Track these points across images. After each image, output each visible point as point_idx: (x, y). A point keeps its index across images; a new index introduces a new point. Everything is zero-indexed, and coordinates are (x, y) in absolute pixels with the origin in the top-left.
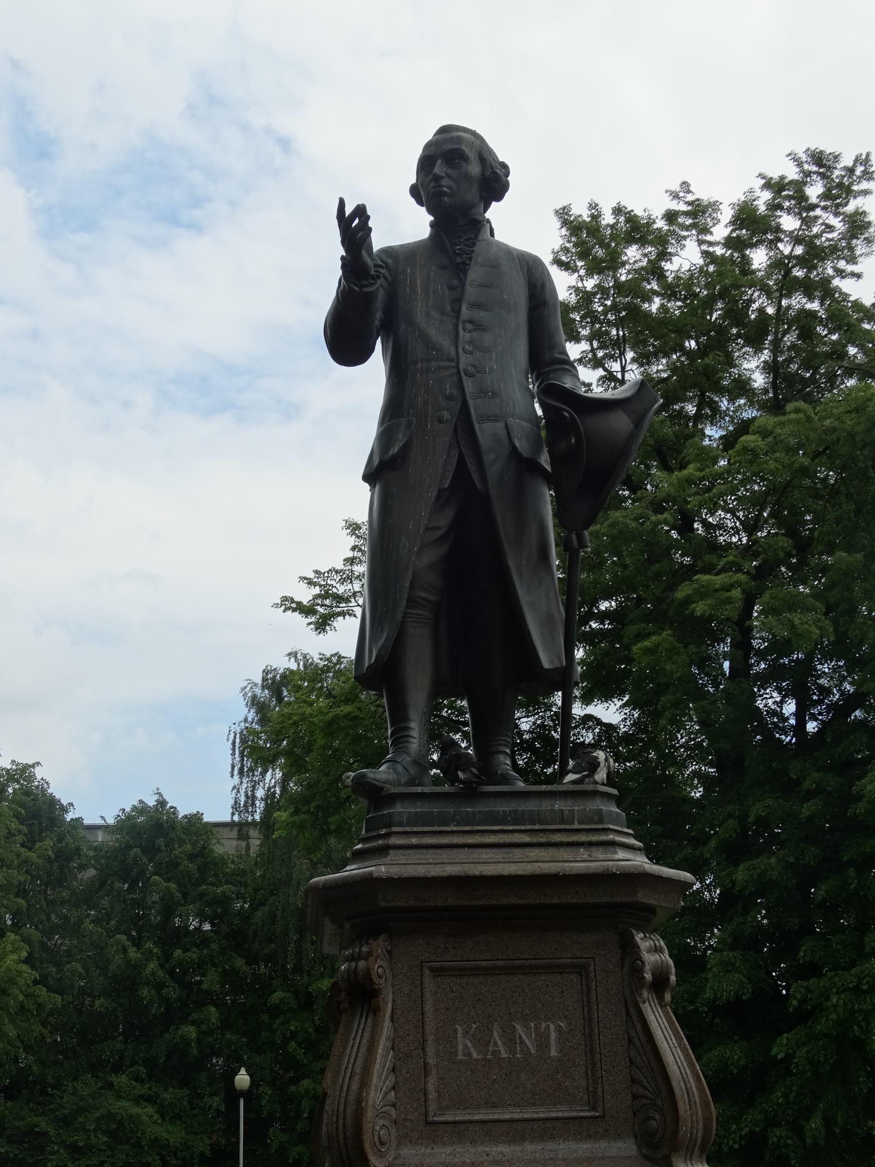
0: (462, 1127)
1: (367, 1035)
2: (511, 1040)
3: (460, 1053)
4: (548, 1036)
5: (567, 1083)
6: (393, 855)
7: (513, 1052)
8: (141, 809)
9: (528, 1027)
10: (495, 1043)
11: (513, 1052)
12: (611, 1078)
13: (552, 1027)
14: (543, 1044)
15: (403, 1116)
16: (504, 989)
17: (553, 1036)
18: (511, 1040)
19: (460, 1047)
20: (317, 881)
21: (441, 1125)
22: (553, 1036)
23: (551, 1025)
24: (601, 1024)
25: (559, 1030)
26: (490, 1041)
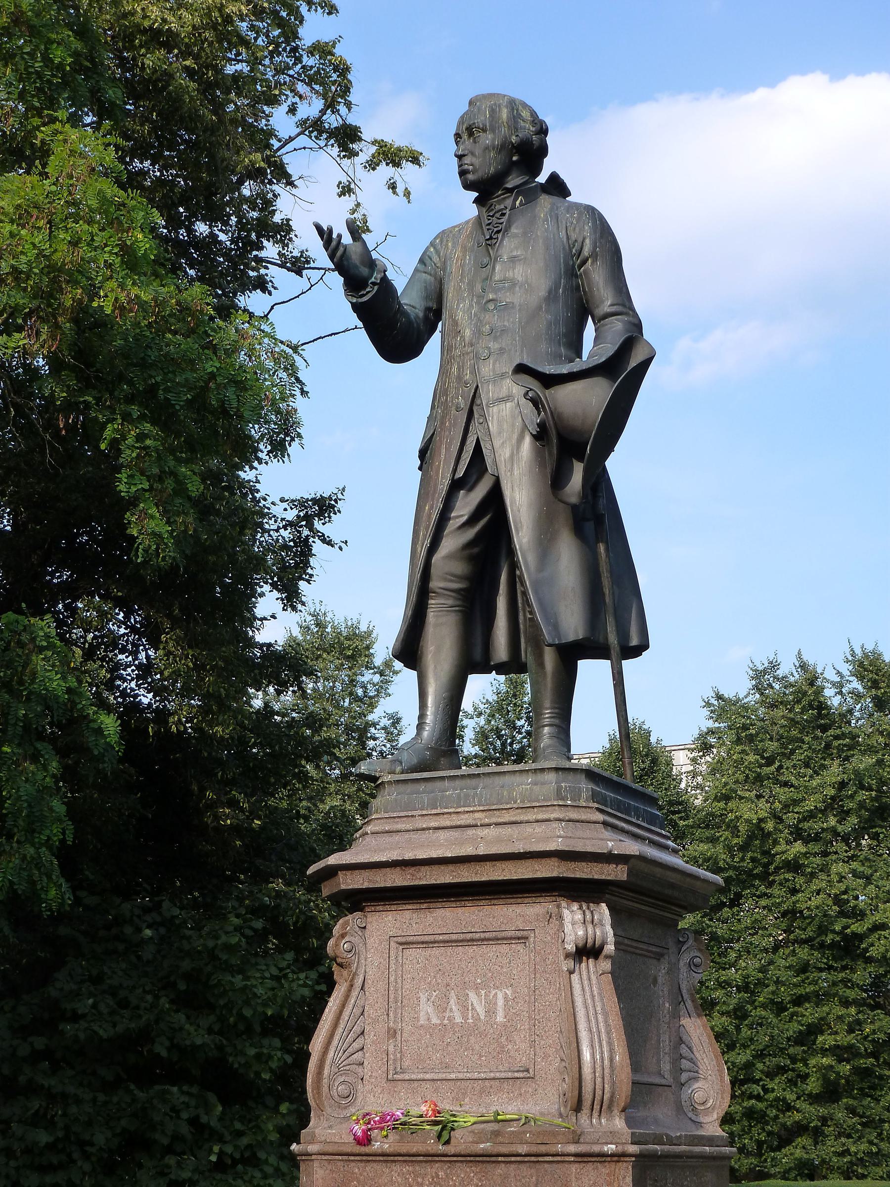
0: (416, 1084)
1: (614, 889)
2: (465, 1008)
3: (422, 1019)
4: (495, 1004)
5: (510, 1047)
6: (373, 823)
7: (465, 1018)
8: (298, 424)
9: (478, 995)
10: (451, 1010)
11: (465, 1018)
12: (543, 1042)
13: (500, 995)
14: (491, 1011)
15: (370, 1074)
16: (460, 960)
17: (500, 1002)
18: (465, 1008)
19: (422, 1014)
20: (549, 634)
21: (399, 1082)
22: (500, 1002)
23: (499, 992)
24: (537, 992)
25: (506, 998)
26: (446, 1008)
